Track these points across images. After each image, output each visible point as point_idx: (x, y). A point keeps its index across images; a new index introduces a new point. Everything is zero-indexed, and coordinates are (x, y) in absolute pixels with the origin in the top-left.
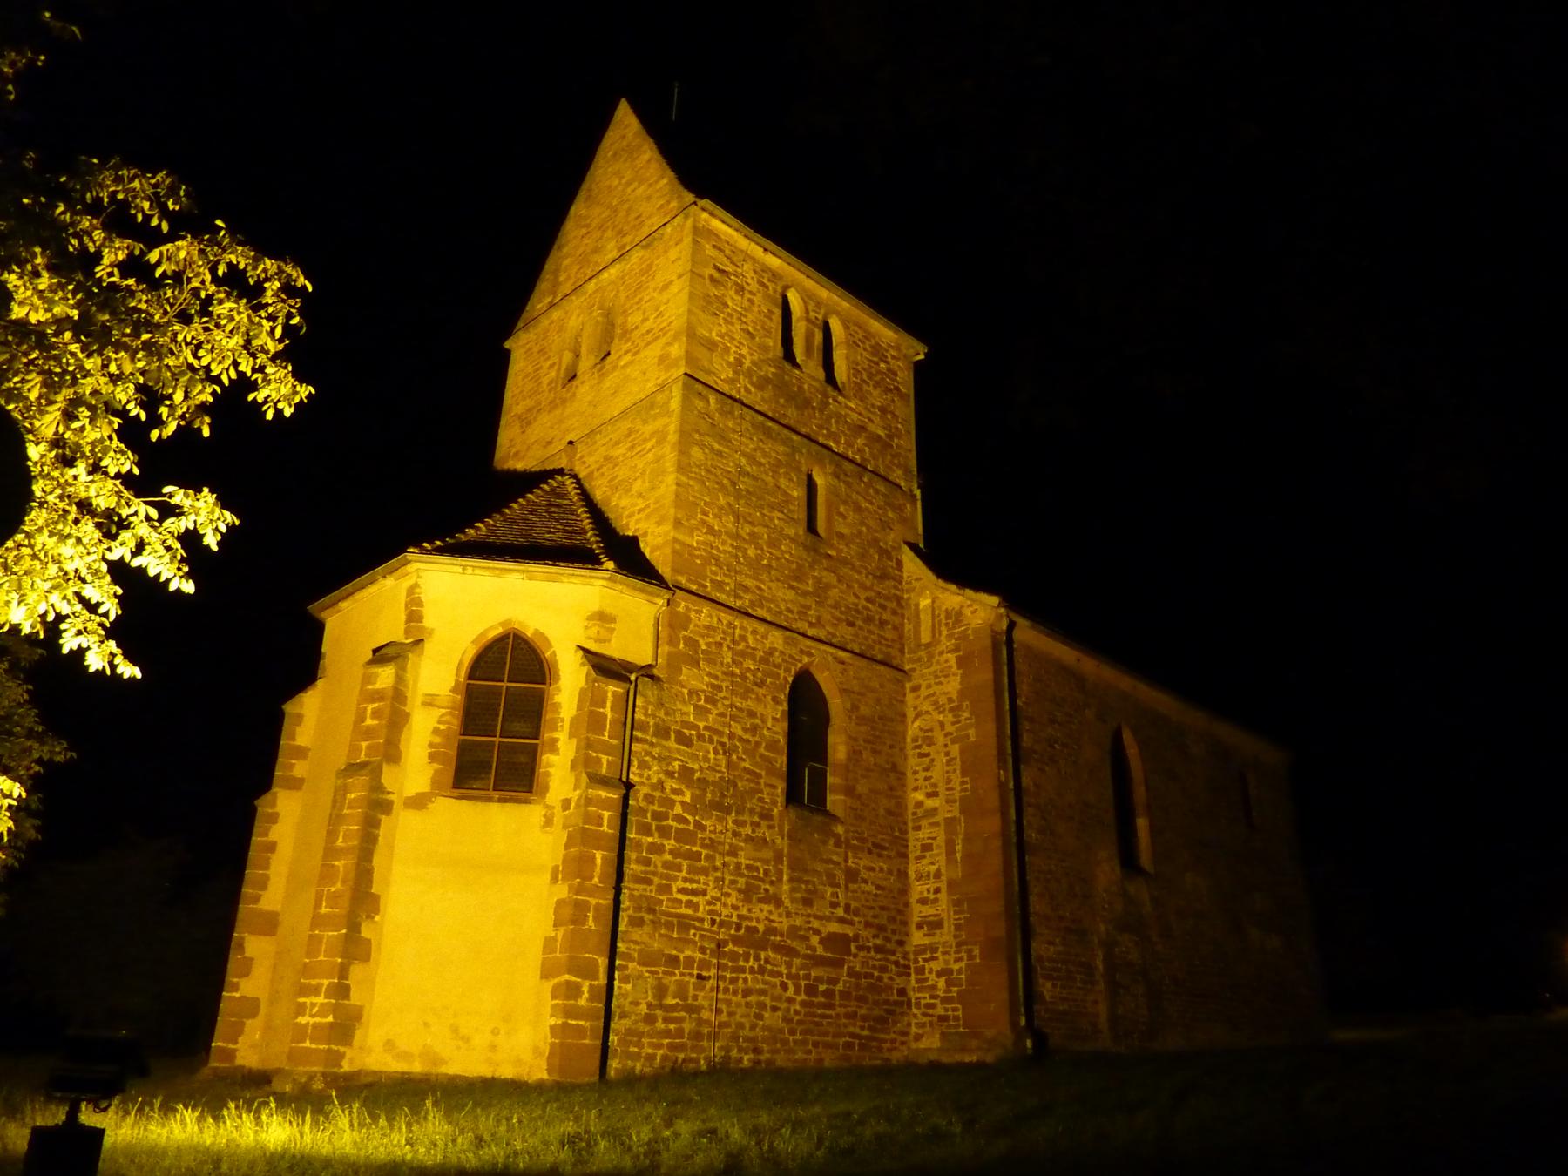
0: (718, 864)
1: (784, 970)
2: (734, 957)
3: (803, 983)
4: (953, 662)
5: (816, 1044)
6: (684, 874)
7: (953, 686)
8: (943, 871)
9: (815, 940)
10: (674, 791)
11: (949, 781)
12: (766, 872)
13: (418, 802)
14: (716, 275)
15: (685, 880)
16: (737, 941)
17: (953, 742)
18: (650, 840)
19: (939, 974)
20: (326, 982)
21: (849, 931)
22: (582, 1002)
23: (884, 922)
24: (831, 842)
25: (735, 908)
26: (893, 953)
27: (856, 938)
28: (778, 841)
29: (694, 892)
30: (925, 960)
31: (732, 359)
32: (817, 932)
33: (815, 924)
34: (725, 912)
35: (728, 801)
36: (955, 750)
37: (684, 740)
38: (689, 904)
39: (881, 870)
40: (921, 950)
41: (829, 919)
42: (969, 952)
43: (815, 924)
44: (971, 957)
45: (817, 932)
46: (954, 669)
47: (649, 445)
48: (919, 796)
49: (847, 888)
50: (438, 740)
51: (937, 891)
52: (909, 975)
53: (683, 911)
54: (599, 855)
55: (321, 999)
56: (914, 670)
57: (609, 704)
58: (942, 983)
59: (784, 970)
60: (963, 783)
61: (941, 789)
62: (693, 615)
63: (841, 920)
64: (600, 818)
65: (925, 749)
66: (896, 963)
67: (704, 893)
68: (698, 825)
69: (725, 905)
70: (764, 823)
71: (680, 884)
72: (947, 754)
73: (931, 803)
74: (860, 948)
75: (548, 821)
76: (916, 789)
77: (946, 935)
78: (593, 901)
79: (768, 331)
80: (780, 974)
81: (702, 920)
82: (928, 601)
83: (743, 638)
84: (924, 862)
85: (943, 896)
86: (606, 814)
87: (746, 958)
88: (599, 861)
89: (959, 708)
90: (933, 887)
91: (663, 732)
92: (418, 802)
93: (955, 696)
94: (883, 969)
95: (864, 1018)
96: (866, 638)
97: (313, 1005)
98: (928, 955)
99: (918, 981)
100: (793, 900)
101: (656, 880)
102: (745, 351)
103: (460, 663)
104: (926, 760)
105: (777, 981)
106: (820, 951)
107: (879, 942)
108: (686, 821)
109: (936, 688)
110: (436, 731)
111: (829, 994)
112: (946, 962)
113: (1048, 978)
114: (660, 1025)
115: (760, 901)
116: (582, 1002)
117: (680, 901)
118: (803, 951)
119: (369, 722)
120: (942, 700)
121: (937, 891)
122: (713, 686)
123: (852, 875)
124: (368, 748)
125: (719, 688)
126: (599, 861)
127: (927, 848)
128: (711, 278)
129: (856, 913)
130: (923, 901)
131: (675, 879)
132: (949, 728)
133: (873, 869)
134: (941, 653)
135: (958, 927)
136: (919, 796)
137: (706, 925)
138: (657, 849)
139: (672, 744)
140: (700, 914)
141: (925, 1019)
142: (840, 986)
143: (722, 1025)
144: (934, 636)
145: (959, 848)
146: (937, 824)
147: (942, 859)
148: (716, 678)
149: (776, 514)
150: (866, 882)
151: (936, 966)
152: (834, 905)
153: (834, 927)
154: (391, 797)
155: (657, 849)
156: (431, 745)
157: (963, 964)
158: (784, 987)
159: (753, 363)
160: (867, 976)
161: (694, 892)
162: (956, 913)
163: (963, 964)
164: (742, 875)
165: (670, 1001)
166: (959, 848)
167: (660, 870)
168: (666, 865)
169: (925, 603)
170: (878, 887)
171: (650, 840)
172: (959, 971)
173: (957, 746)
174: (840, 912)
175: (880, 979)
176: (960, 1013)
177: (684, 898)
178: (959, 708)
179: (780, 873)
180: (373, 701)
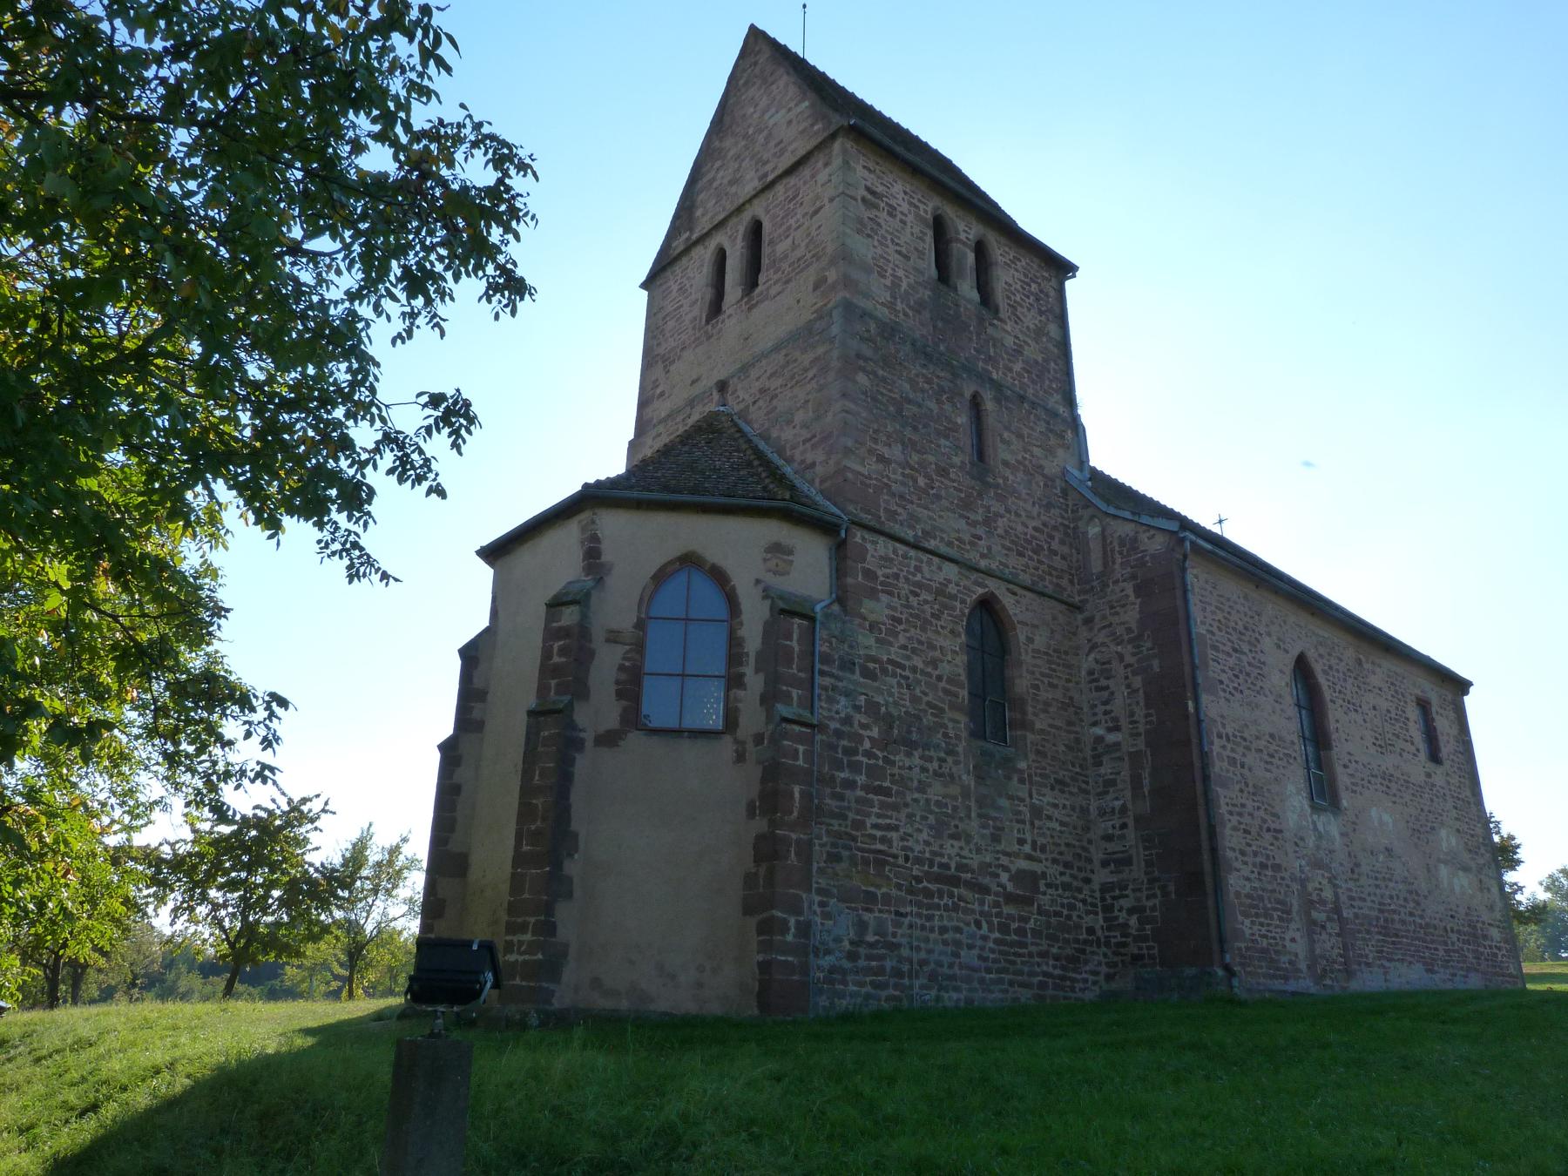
0: (909, 799)
1: (976, 907)
2: (929, 894)
3: (996, 921)
4: (1130, 591)
5: (1011, 983)
6: (876, 810)
7: (1131, 616)
8: (1130, 806)
9: (1004, 877)
10: (864, 726)
11: (1132, 714)
12: (955, 808)
13: (609, 739)
14: (869, 197)
15: (879, 816)
16: (930, 877)
17: (1135, 673)
18: (842, 775)
19: (1131, 911)
20: (532, 920)
21: (1037, 867)
22: (790, 938)
23: (1069, 858)
24: (1015, 779)
25: (927, 843)
26: (1080, 890)
27: (1044, 875)
28: (964, 777)
29: (889, 828)
30: (1114, 898)
31: (888, 282)
32: (1006, 869)
33: (1004, 860)
34: (917, 848)
35: (914, 737)
36: (1137, 682)
37: (867, 674)
38: (883, 840)
39: (1064, 806)
40: (1106, 888)
41: (1017, 855)
42: (1163, 888)
43: (1004, 860)
44: (1165, 894)
45: (1006, 869)
46: (1132, 598)
47: (810, 374)
48: (1099, 731)
49: (1032, 824)
50: (623, 677)
51: (1124, 826)
52: (1096, 914)
53: (879, 846)
54: (797, 790)
55: (528, 937)
56: (1085, 602)
57: (795, 637)
58: (1133, 921)
59: (976, 907)
60: (1146, 716)
61: (1124, 723)
62: (869, 546)
63: (1029, 857)
64: (796, 751)
65: (1103, 682)
66: (1084, 901)
67: (896, 828)
68: (886, 760)
69: (917, 841)
70: (950, 759)
71: (874, 820)
72: (1128, 686)
73: (1112, 738)
74: (1049, 886)
75: (740, 757)
76: (1095, 724)
77: (1137, 871)
78: (794, 836)
79: (921, 254)
80: (973, 911)
81: (895, 857)
82: (1097, 529)
83: (918, 569)
84: (1108, 797)
85: (1131, 833)
86: (801, 748)
87: (941, 895)
88: (797, 795)
89: (1140, 636)
90: (1118, 823)
91: (847, 665)
92: (609, 739)
93: (1134, 626)
94: (1072, 907)
95: (1057, 958)
96: (1036, 569)
97: (521, 943)
98: (1117, 892)
99: (1105, 920)
100: (983, 836)
101: (851, 815)
102: (900, 273)
103: (641, 599)
104: (1106, 694)
105: (970, 918)
106: (1010, 887)
107: (1066, 879)
108: (877, 758)
109: (1115, 620)
110: (621, 668)
111: (1021, 932)
112: (1138, 900)
113: (1246, 915)
114: (862, 963)
115: (952, 837)
116: (790, 938)
117: (874, 837)
118: (994, 888)
119: (556, 659)
120: (1120, 630)
121: (1124, 826)
122: (894, 618)
123: (1037, 812)
124: (557, 685)
125: (899, 621)
126: (797, 795)
127: (1113, 783)
128: (864, 200)
129: (1043, 849)
130: (1108, 838)
131: (869, 815)
132: (1129, 659)
133: (1055, 806)
134: (1117, 582)
135: (1149, 864)
136: (1099, 731)
137: (901, 861)
138: (850, 784)
139: (857, 677)
140: (894, 851)
141: (1116, 959)
142: (1031, 924)
143: (922, 963)
144: (1105, 565)
145: (1146, 782)
146: (1121, 759)
147: (1128, 794)
148: (894, 609)
149: (943, 442)
150: (1049, 818)
151: (1126, 903)
152: (1021, 842)
153: (1023, 864)
154: (582, 735)
155: (850, 784)
156: (617, 682)
157: (1157, 901)
158: (978, 924)
159: (909, 285)
160: (1057, 914)
161: (889, 828)
162: (1145, 848)
163: (1157, 901)
164: (931, 812)
165: (871, 938)
166: (1146, 782)
167: (853, 805)
168: (858, 800)
169: (1094, 530)
170: (1062, 824)
171: (842, 775)
172: (1153, 909)
173: (1139, 678)
174: (1027, 848)
175: (1069, 917)
176: (1156, 951)
177: (879, 834)
178: (1140, 636)
179: (969, 809)
180: (559, 639)
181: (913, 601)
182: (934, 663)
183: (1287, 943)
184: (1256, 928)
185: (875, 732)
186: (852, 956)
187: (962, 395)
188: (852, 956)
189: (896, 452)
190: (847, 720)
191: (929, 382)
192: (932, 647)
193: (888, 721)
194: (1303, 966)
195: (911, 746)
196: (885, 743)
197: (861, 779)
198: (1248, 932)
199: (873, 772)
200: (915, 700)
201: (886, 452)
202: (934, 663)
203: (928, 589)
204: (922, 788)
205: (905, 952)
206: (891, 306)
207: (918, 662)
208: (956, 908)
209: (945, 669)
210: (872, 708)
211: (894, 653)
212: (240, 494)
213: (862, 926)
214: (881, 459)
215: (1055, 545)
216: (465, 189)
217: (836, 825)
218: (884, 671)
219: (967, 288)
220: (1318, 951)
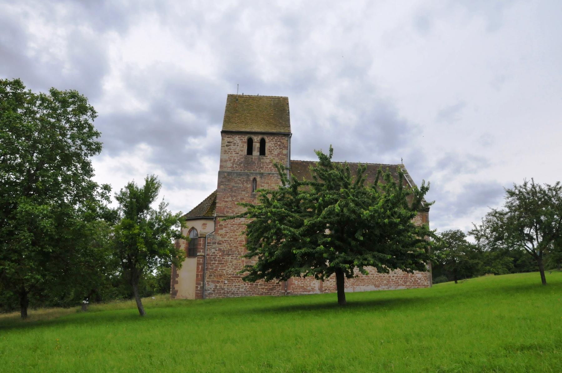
37: (219, 244)
91: (215, 243)
138: (215, 263)
139: (217, 245)
149: (243, 193)
155: (215, 263)
165: (218, 288)
181: (232, 228)
182: (236, 239)
183: (312, 285)
184: (300, 283)
185: (220, 254)
186: (214, 291)
187: (250, 180)
188: (214, 291)
189: (230, 199)
190: (214, 253)
191: (240, 180)
192: (236, 235)
193: (224, 251)
194: (317, 288)
195: (229, 255)
196: (223, 255)
197: (217, 262)
198: (296, 284)
199: (219, 261)
200: (230, 246)
201: (227, 200)
202: (236, 239)
203: (236, 224)
204: (231, 262)
205: (226, 290)
206: (232, 167)
207: (232, 239)
208: (239, 282)
209: (239, 239)
210: (220, 250)
211: (226, 239)
212: (259, 261)
213: (216, 286)
214: (226, 202)
215: (241, 290)
216: (259, 265)
217: (211, 270)
218: (223, 242)
219: (256, 153)
220: (324, 285)
